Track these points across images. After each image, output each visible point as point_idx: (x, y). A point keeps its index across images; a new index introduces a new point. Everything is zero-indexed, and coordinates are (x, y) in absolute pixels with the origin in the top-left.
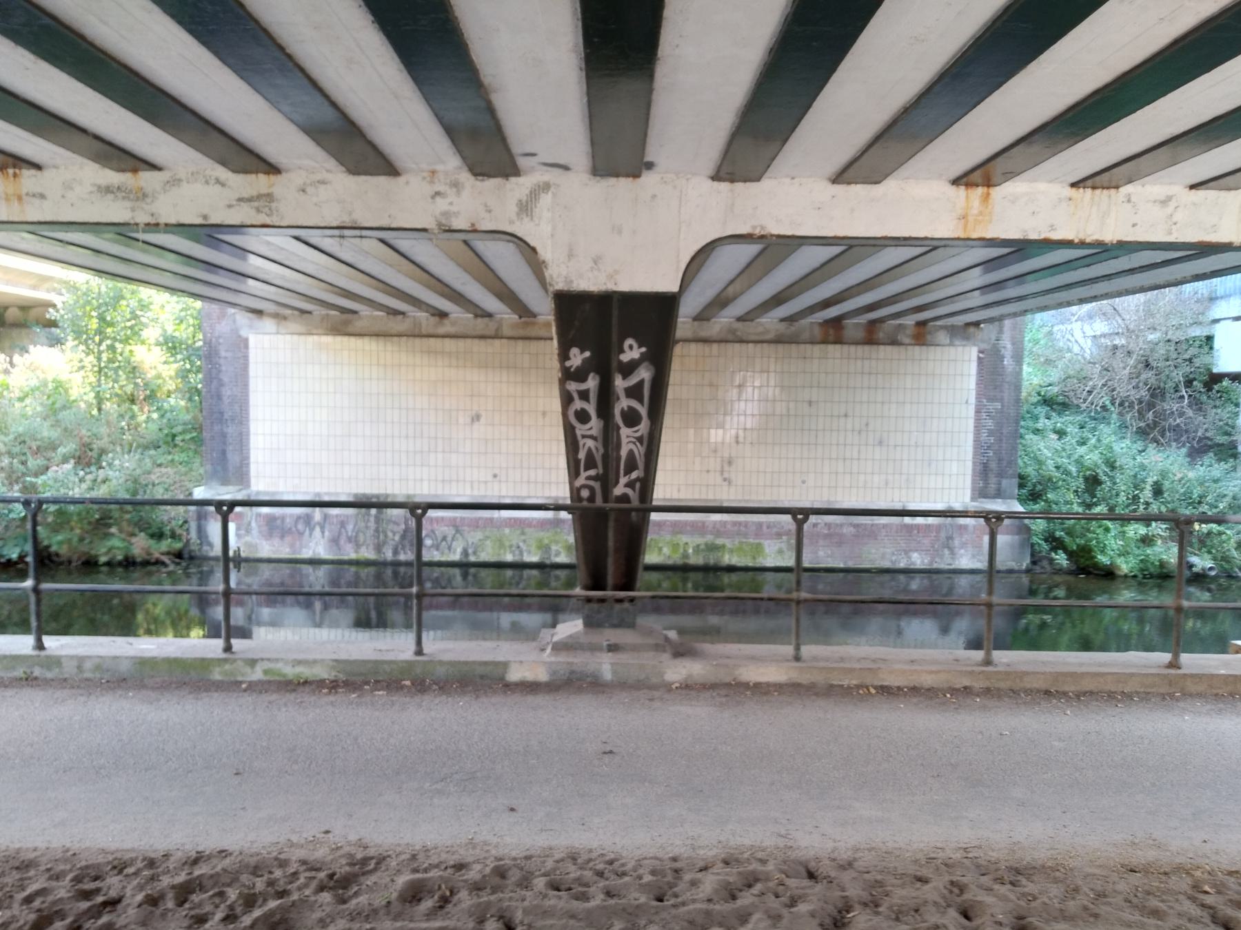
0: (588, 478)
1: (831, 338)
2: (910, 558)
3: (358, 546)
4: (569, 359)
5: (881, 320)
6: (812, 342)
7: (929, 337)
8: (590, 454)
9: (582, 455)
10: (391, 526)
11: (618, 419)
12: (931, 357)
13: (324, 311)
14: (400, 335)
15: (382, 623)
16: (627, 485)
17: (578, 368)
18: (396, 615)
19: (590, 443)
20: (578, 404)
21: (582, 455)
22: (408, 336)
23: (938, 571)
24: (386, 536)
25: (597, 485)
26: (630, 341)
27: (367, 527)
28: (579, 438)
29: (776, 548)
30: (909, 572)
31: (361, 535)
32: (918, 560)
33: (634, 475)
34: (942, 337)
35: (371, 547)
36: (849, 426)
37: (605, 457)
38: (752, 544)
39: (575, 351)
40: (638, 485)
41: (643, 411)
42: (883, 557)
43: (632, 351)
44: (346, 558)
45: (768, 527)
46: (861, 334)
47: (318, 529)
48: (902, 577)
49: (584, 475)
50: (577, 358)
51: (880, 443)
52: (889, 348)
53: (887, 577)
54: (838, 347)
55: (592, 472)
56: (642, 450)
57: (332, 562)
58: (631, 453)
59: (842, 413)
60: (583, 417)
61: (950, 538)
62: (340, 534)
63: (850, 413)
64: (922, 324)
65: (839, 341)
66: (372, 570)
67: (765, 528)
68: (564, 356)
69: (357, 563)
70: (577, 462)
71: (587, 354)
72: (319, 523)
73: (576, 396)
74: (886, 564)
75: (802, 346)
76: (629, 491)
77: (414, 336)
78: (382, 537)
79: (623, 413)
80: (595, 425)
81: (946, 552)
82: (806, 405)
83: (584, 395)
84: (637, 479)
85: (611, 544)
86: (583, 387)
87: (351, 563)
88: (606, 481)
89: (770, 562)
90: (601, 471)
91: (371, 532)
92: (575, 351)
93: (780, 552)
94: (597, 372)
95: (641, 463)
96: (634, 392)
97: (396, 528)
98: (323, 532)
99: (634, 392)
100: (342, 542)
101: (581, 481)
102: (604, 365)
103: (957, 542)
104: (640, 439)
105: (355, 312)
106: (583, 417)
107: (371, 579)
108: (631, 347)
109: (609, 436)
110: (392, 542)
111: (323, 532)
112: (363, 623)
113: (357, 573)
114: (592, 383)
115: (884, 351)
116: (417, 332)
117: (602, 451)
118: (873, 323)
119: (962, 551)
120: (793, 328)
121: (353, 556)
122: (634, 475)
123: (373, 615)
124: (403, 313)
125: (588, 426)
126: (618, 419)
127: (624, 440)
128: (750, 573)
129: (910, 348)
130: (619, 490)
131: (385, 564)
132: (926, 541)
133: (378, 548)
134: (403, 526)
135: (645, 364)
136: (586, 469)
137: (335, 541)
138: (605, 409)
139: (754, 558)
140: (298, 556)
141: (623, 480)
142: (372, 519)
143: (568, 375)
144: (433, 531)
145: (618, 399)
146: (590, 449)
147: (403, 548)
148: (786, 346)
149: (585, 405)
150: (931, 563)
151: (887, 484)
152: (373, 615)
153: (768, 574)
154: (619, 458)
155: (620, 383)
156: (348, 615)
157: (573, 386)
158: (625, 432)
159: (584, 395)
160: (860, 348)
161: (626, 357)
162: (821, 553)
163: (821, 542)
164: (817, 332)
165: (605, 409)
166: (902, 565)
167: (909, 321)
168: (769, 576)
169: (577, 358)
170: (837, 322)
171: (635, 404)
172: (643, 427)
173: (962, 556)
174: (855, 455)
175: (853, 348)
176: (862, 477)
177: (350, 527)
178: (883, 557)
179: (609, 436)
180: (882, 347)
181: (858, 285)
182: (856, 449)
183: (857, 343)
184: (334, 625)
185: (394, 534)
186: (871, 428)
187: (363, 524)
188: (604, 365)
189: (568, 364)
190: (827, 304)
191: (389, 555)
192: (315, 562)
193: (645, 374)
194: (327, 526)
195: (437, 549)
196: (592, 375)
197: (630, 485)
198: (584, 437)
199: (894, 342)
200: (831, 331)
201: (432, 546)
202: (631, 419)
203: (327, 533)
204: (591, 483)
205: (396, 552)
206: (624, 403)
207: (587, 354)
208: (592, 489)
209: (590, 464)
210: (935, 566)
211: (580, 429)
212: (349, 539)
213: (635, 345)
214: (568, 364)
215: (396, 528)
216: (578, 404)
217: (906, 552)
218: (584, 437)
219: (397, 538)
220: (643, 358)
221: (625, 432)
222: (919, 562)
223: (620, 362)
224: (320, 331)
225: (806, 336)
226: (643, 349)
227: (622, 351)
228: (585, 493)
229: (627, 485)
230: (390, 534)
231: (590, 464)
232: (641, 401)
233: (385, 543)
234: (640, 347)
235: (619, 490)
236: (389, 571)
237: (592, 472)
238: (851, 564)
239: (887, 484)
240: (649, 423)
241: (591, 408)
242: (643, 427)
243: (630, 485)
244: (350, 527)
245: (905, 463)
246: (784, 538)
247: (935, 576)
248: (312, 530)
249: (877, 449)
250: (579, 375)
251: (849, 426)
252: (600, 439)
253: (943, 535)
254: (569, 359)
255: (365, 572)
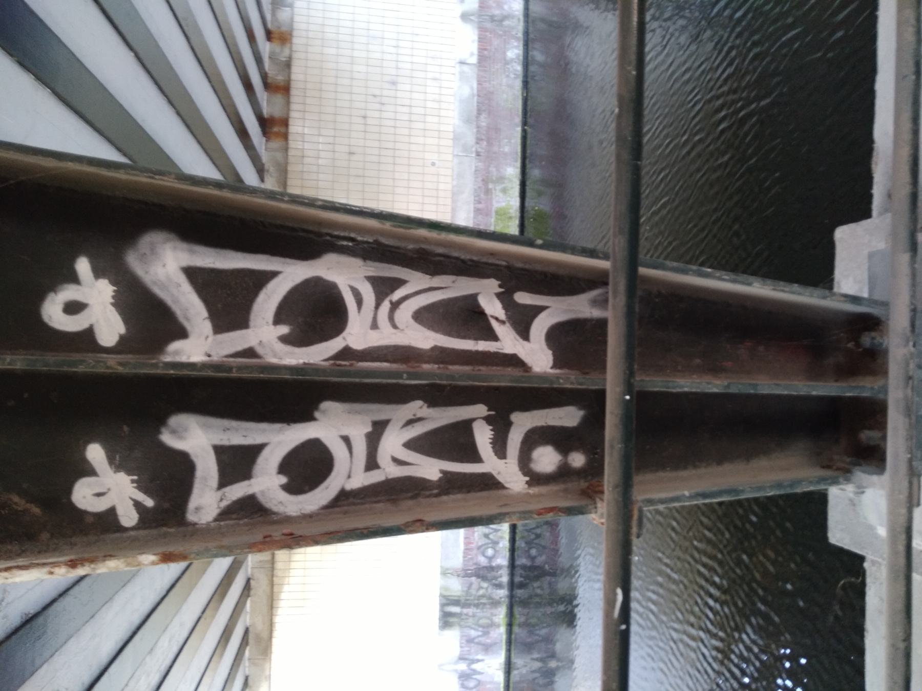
0: (500, 449)
1: (283, 130)
2: (512, 60)
3: (493, 625)
4: (112, 512)
5: (264, 77)
6: (286, 149)
7: (284, 29)
8: (426, 445)
9: (430, 469)
10: (473, 591)
11: (318, 354)
12: (304, 26)
13: (246, 662)
14: (272, 584)
15: (569, 599)
16: (524, 333)
17: (142, 486)
18: (562, 586)
19: (393, 443)
20: (266, 482)
21: (430, 469)
22: (273, 576)
23: (526, 33)
24: (483, 596)
25: (523, 423)
26: (53, 312)
27: (474, 616)
28: (375, 477)
29: (501, 195)
30: (527, 62)
31: (482, 622)
32: (515, 52)
33: (493, 307)
34: (283, 15)
35: (494, 611)
36: (377, 114)
37: (438, 395)
38: (497, 219)
39: (84, 495)
40: (523, 298)
41: (291, 274)
42: (510, 86)
43: (87, 305)
44: (504, 637)
45: (480, 203)
46: (279, 99)
47: (474, 666)
48: (532, 68)
49: (490, 464)
50: (108, 487)
51: (394, 83)
52: (294, 69)
53: (532, 85)
54: (291, 122)
55: (483, 436)
56: (416, 280)
57: (509, 651)
58: (421, 316)
59: (361, 121)
60: (308, 466)
61: (492, 19)
62: (479, 643)
63: (362, 113)
64: (269, 35)
65: (285, 122)
66: (517, 610)
67: (480, 206)
68: (98, 533)
69: (510, 625)
70: (451, 484)
71: (95, 453)
72: (469, 665)
73: (237, 491)
74: (518, 84)
75: (291, 159)
76: (540, 326)
77: (273, 568)
78: (484, 601)
79: (296, 340)
80: (336, 427)
81: (506, 23)
82: (354, 157)
83: (237, 463)
84: (505, 298)
85: (713, 385)
86: (207, 468)
87: (510, 632)
88: (510, 395)
89: (515, 202)
90: (481, 410)
91: (478, 612)
92: (84, 495)
93: (504, 191)
94: (161, 421)
95: (457, 287)
96: (229, 301)
97: (475, 586)
98: (478, 661)
99: (229, 301)
100: (489, 641)
101: (508, 472)
102: (135, 400)
103: (497, 12)
104: (384, 287)
105: (247, 631)
106: (308, 466)
107: (526, 611)
108: (74, 308)
109: (368, 384)
110: (490, 590)
111: (478, 661)
112: (569, 619)
113: (520, 625)
114: (195, 437)
115: (297, 74)
116: (269, 565)
117: (416, 407)
118: (267, 85)
119: (506, 7)
120: (272, 169)
121: (503, 630)
122: (493, 307)
123: (561, 608)
124: (248, 581)
125: (338, 451)
126: (318, 354)
127: (386, 337)
128: (526, 222)
129: (294, 48)
130: (538, 356)
131: (511, 597)
132: (496, 42)
133: (495, 603)
134: (473, 579)
135: (133, 260)
136: (474, 456)
137: (487, 648)
138: (291, 397)
139: (511, 218)
140: (502, 685)
141: (508, 341)
142: (465, 611)
143: (166, 518)
144: (479, 548)
145: (250, 353)
146: (411, 445)
147: (496, 578)
148: (289, 176)
149: (270, 460)
150: (517, 39)
151: (435, 79)
152: (561, 608)
153: (527, 204)
154: (442, 355)
155: (199, 345)
156: (562, 633)
157: (206, 501)
158: (358, 334)
159: (237, 463)
160: (293, 99)
161: (109, 327)
162: (507, 149)
163: (495, 149)
164: (276, 144)
165: (291, 397)
166: (519, 68)
167: (265, 47)
168: (529, 203)
169: (108, 487)
170: (265, 123)
171: (268, 301)
172: (345, 274)
173: (510, 8)
174: (406, 109)
175: (293, 107)
176: (429, 104)
177: (473, 633)
178: (510, 86)
179: (368, 384)
180: (293, 77)
181: (210, 82)
182: (400, 109)
183: (288, 103)
184: (569, 647)
185: (481, 588)
186: (377, 92)
187: (471, 620)
188: (135, 400)
189: (128, 518)
190: (242, 133)
191: (503, 593)
192: (509, 668)
193: (166, 265)
194: (471, 657)
195: (497, 543)
196: (167, 438)
197: (522, 322)
198: (372, 464)
199: (288, 65)
200: (276, 129)
201: (493, 548)
202: (316, 312)
203: (479, 657)
204: (515, 438)
205: (499, 586)
206: (265, 336)
207: (95, 453)
208: (534, 439)
209: (454, 442)
210: (520, 35)
211: (349, 473)
212: (486, 634)
213: (68, 293)
214: (128, 518)
215: (475, 586)
216: (266, 482)
217: (507, 62)
218: (372, 464)
219: (485, 585)
220: (111, 267)
221: (358, 334)
222: (516, 51)
223: (123, 345)
224: (267, 666)
225: (279, 156)
226: (83, 266)
227: (87, 338)
228: (546, 459)
229: (524, 333)
230: (481, 592)
231: (454, 442)
232: (262, 279)
233: (490, 598)
234: (74, 279)
235: (538, 356)
236: (519, 592)
237: (483, 436)
238: (518, 119)
239: (435, 79)
240: (331, 258)
241: (280, 440)
242: (345, 274)
243: (522, 322)
244: (473, 633)
245: (415, 59)
246: (491, 186)
247: (531, 36)
248: (475, 672)
249: (400, 87)
250: (169, 479)
251: (377, 114)
252: (382, 411)
253: (489, 25)
254: (112, 512)
255: (519, 618)
